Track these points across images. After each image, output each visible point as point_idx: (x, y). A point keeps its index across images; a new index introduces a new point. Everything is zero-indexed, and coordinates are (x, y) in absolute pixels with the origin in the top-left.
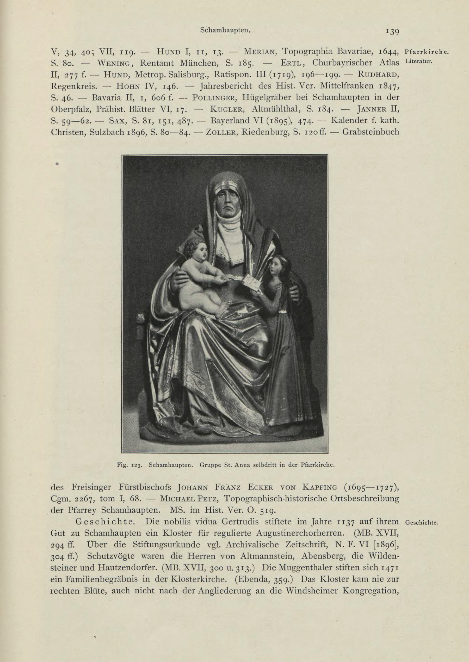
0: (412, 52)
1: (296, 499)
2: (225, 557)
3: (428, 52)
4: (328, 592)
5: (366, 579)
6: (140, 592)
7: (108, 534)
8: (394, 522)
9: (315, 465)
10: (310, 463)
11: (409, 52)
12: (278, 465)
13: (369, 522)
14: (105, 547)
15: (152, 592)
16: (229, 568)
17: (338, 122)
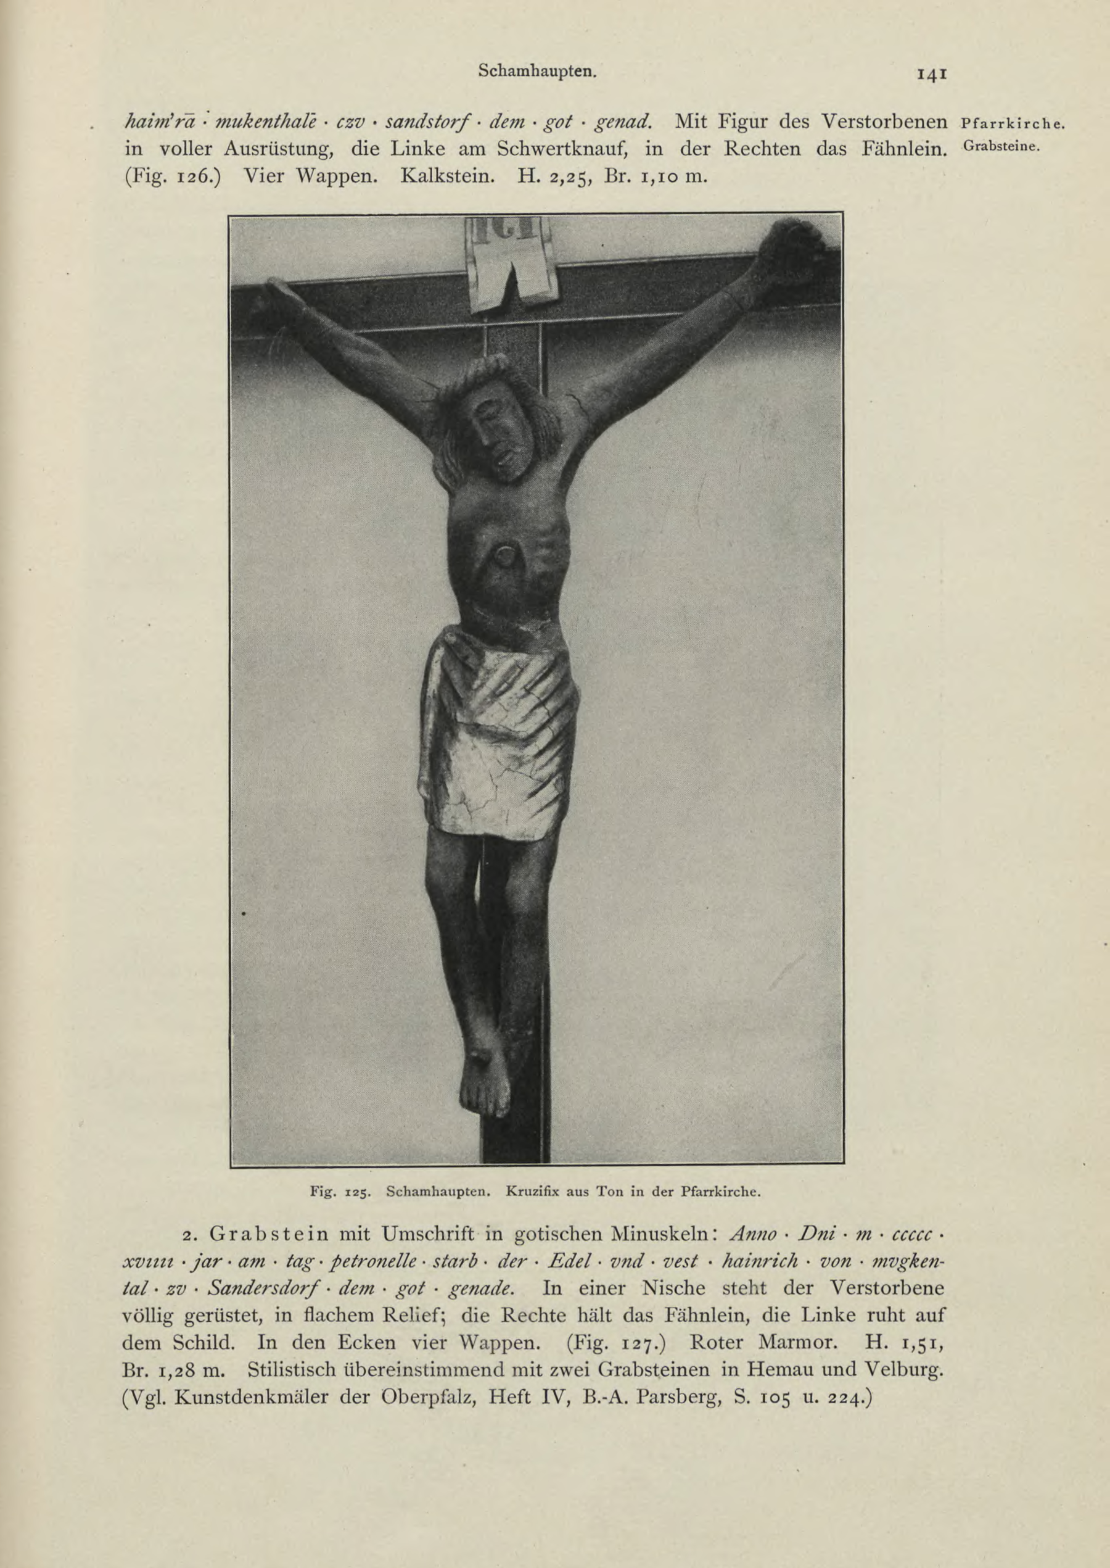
0: (979, 124)
3: (1016, 125)
9: (714, 1193)
10: (701, 1187)
12: (627, 1192)
13: (938, 1317)
14: (324, 1402)
15: (760, 1291)
16: (808, 1397)
17: (416, 179)
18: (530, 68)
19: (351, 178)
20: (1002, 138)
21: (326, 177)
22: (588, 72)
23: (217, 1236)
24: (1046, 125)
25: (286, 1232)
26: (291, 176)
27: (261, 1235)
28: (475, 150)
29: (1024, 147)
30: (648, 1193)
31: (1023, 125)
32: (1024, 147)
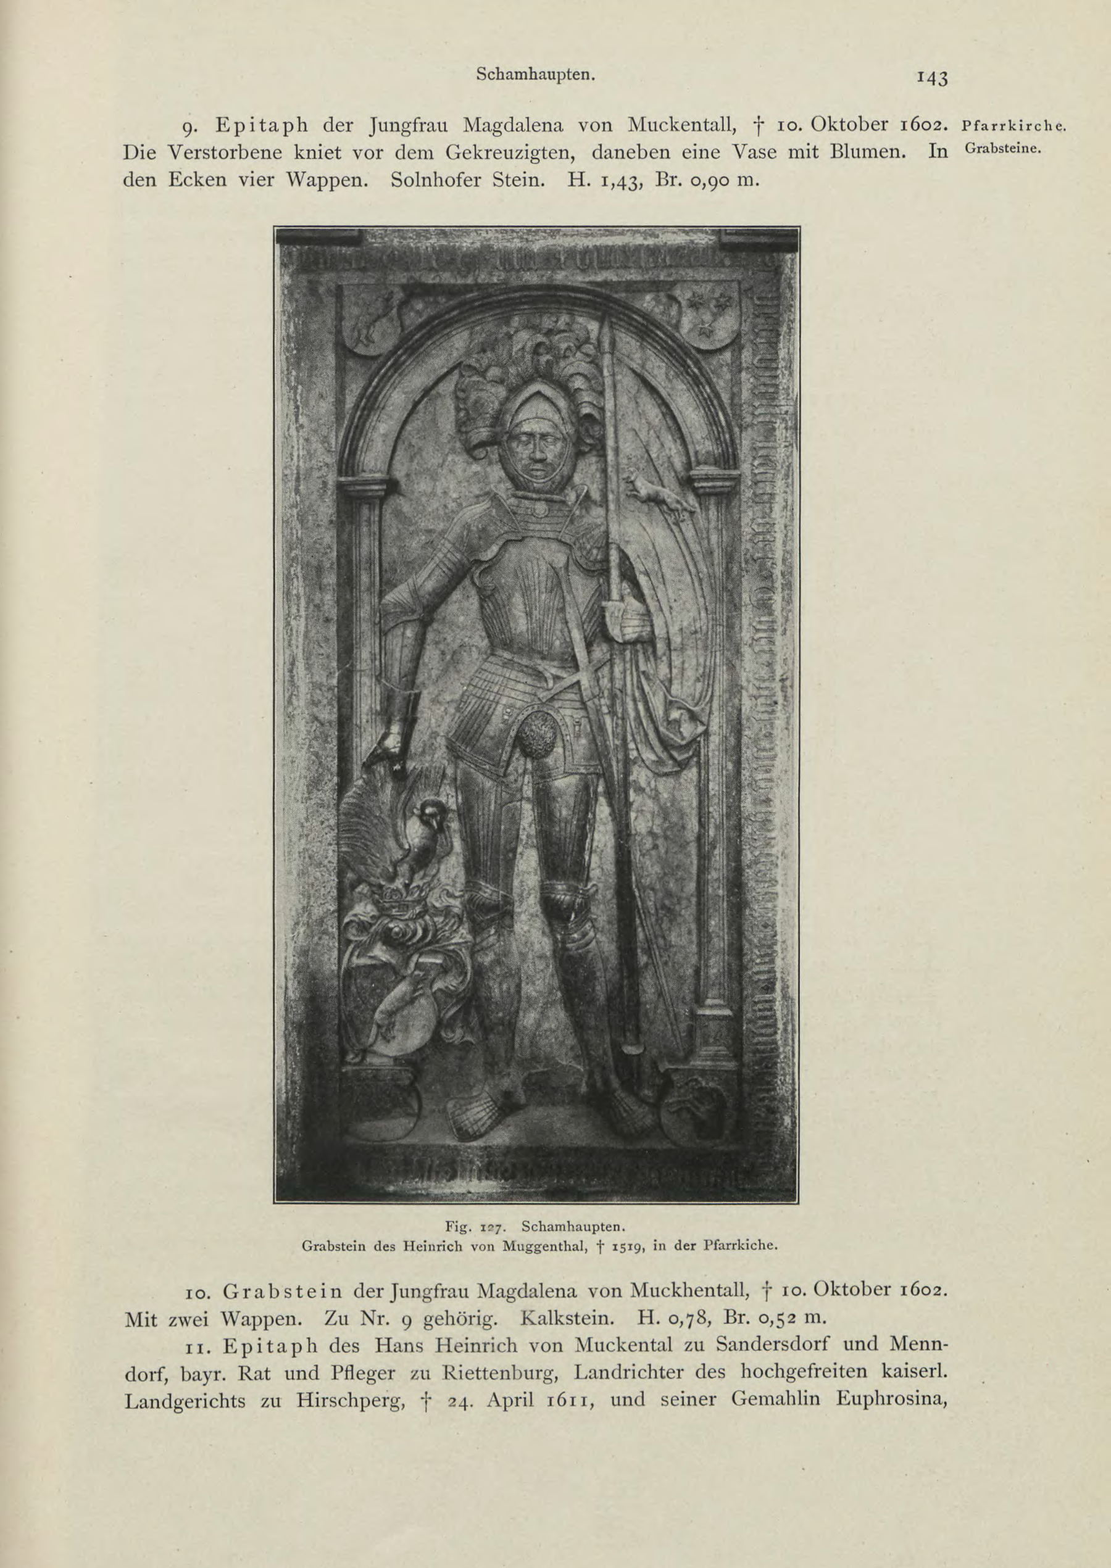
0: (979, 127)
1: (211, 153)
2: (362, 155)
3: (1017, 127)
4: (873, 154)
5: (429, 153)
6: (318, 156)
7: (800, 155)
8: (423, 153)
9: (736, 1247)
11: (973, 126)
18: (528, 71)
19: (341, 182)
20: (1005, 140)
21: (317, 181)
22: (585, 76)
23: (230, 1294)
24: (1048, 127)
25: (299, 1289)
26: (487, 181)
27: (274, 1293)
28: (867, 152)
29: (1026, 149)
30: (670, 1246)
31: (1025, 127)
32: (1026, 149)
